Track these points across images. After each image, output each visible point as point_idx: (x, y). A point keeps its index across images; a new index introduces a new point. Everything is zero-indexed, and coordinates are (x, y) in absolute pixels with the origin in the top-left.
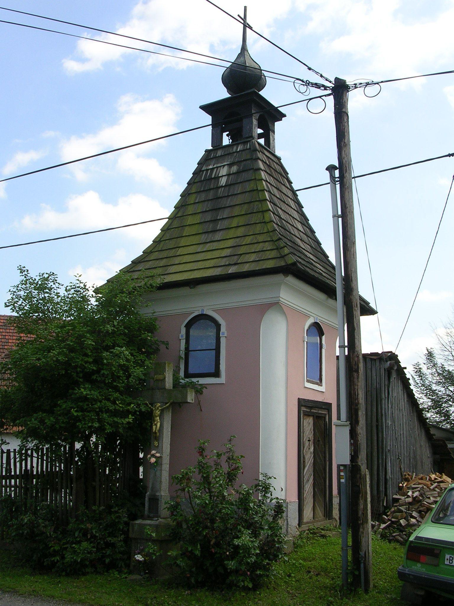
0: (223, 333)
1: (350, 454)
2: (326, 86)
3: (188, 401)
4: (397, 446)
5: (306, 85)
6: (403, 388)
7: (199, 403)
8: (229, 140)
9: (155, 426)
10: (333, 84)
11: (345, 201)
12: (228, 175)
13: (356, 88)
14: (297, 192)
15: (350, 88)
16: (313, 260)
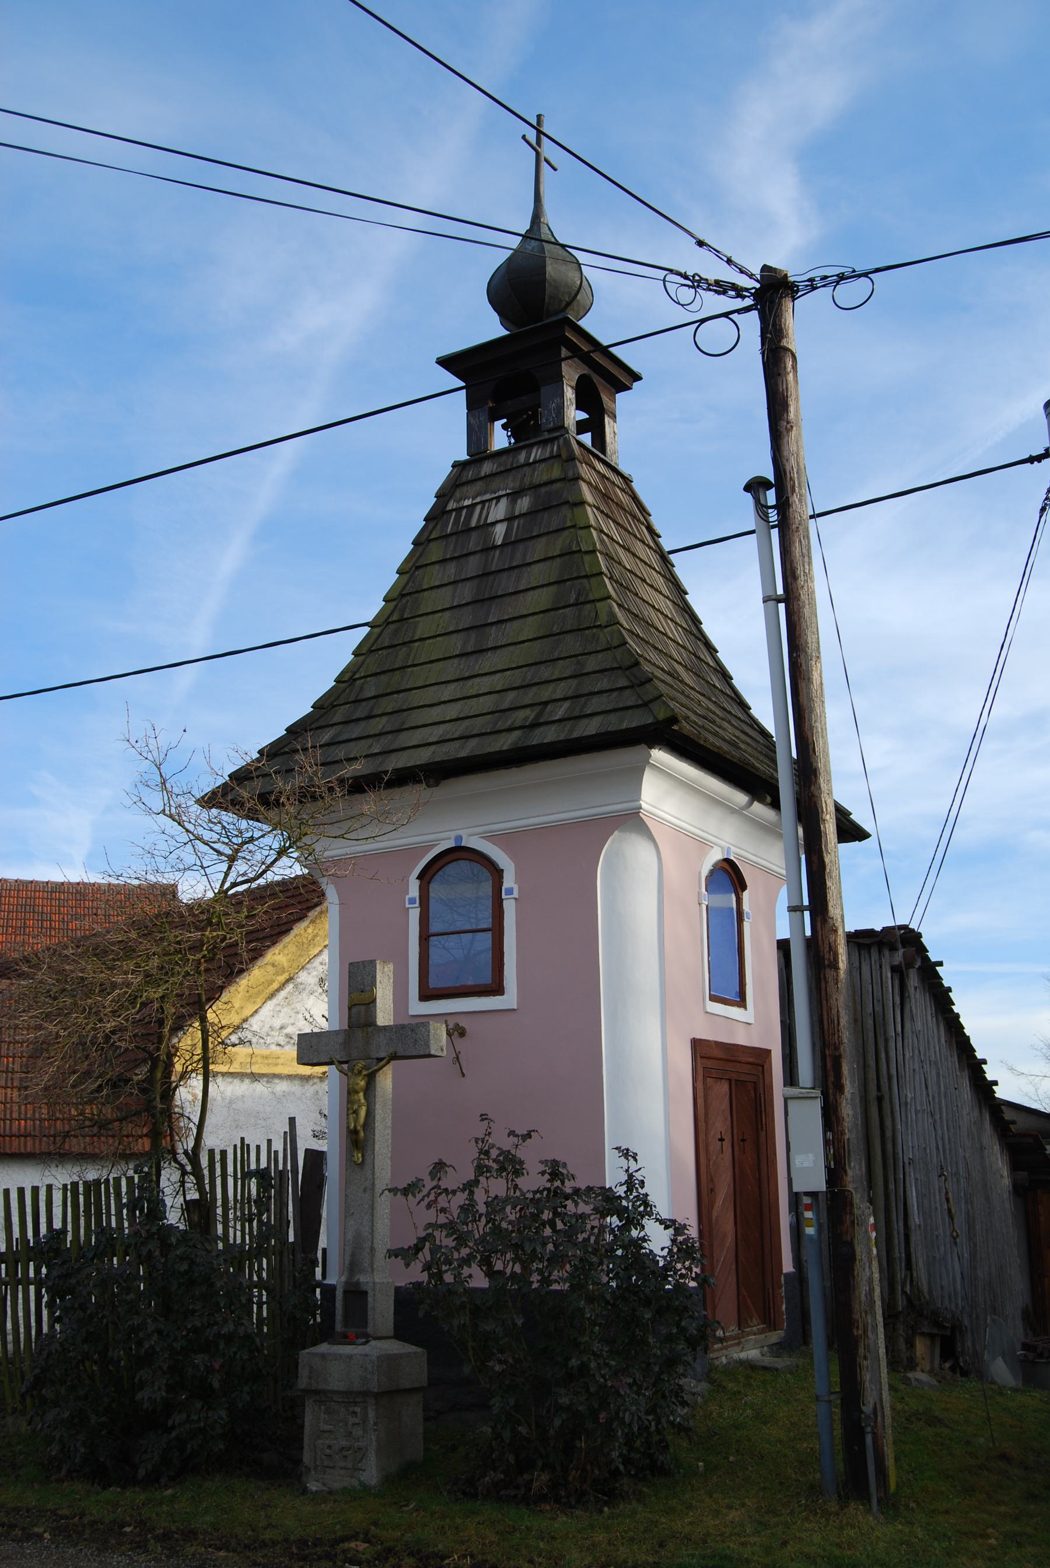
0: (510, 891)
1: (825, 1167)
2: (742, 288)
3: (433, 1052)
4: (928, 1150)
5: (693, 287)
6: (935, 1007)
7: (458, 1058)
8: (508, 437)
9: (354, 1115)
10: (757, 281)
11: (792, 562)
12: (509, 519)
13: (814, 288)
14: (671, 556)
15: (798, 291)
16: (714, 713)
